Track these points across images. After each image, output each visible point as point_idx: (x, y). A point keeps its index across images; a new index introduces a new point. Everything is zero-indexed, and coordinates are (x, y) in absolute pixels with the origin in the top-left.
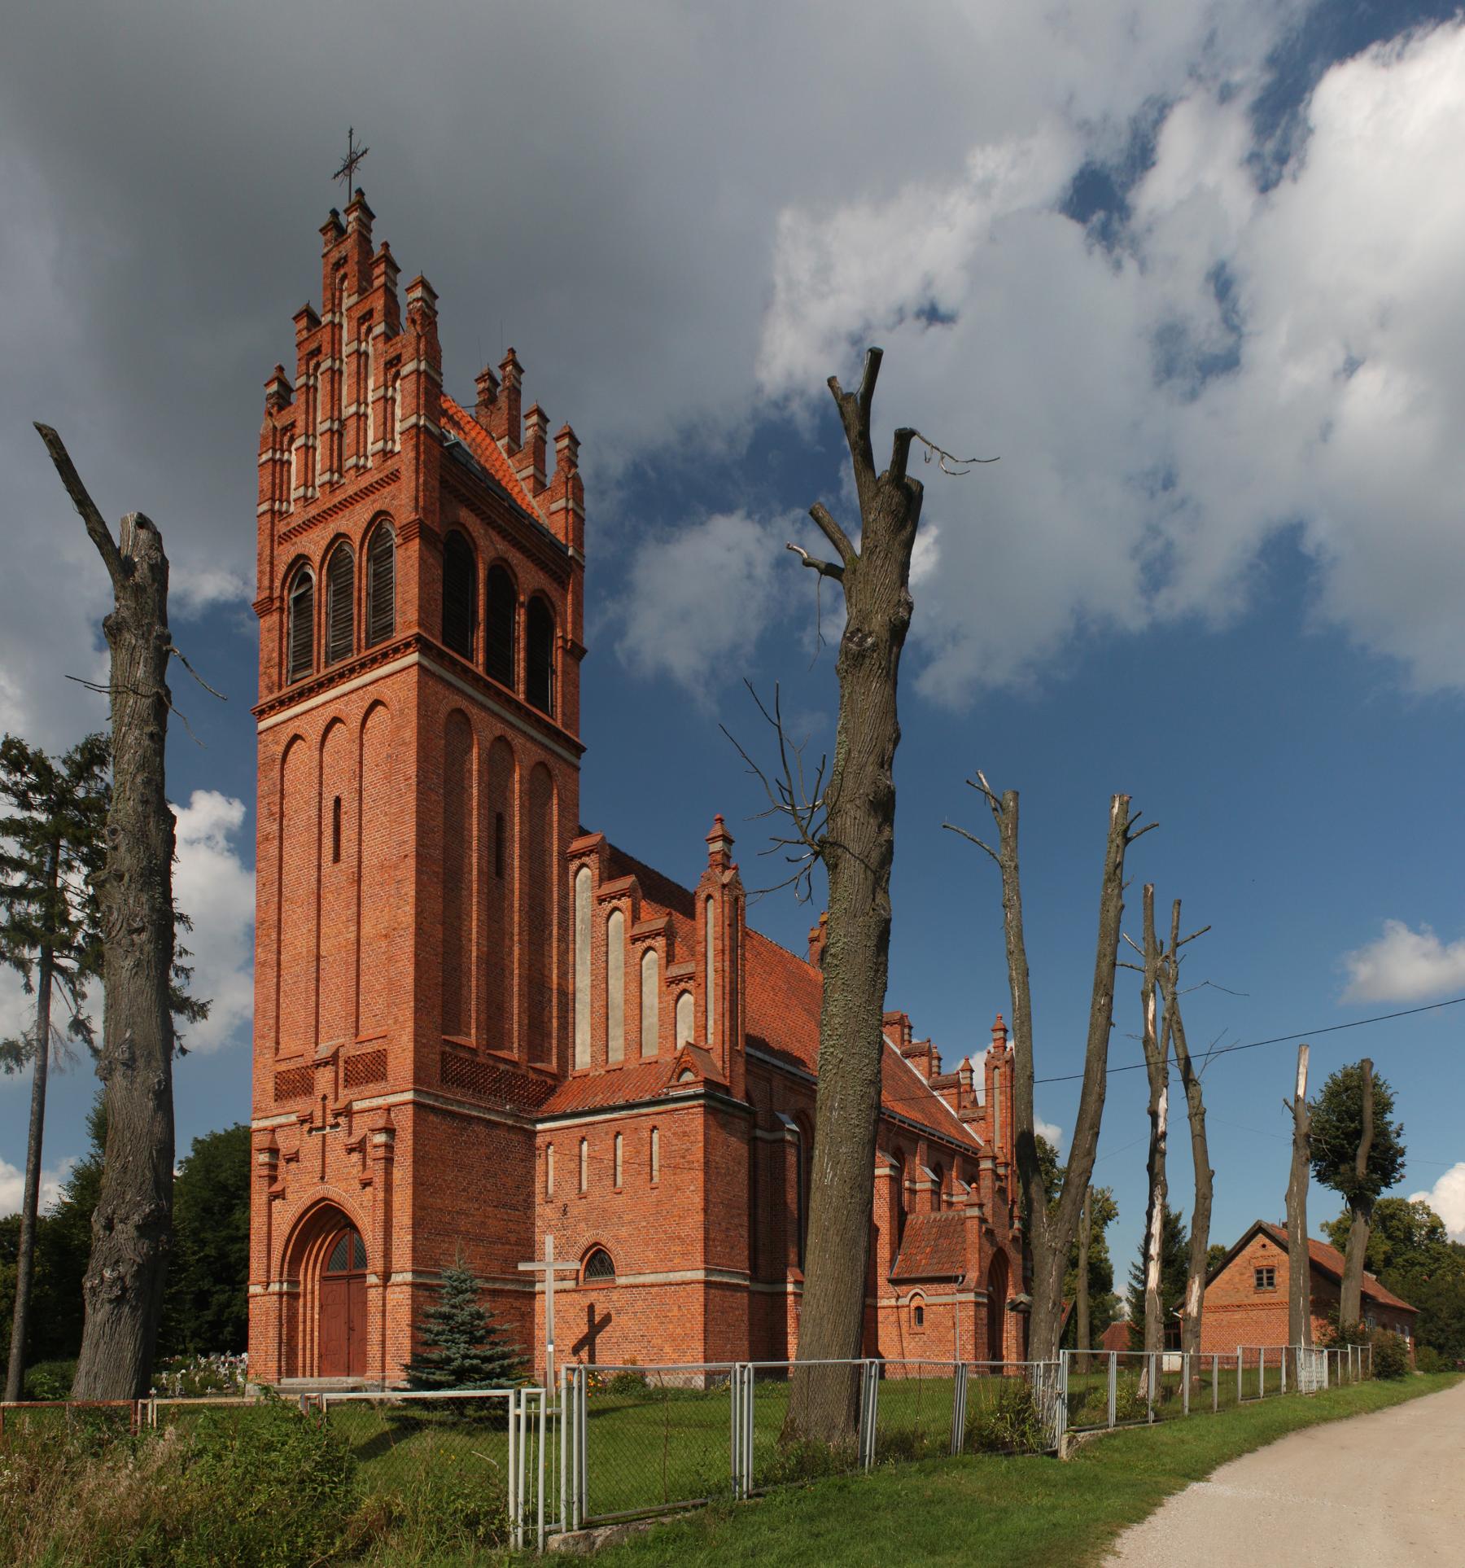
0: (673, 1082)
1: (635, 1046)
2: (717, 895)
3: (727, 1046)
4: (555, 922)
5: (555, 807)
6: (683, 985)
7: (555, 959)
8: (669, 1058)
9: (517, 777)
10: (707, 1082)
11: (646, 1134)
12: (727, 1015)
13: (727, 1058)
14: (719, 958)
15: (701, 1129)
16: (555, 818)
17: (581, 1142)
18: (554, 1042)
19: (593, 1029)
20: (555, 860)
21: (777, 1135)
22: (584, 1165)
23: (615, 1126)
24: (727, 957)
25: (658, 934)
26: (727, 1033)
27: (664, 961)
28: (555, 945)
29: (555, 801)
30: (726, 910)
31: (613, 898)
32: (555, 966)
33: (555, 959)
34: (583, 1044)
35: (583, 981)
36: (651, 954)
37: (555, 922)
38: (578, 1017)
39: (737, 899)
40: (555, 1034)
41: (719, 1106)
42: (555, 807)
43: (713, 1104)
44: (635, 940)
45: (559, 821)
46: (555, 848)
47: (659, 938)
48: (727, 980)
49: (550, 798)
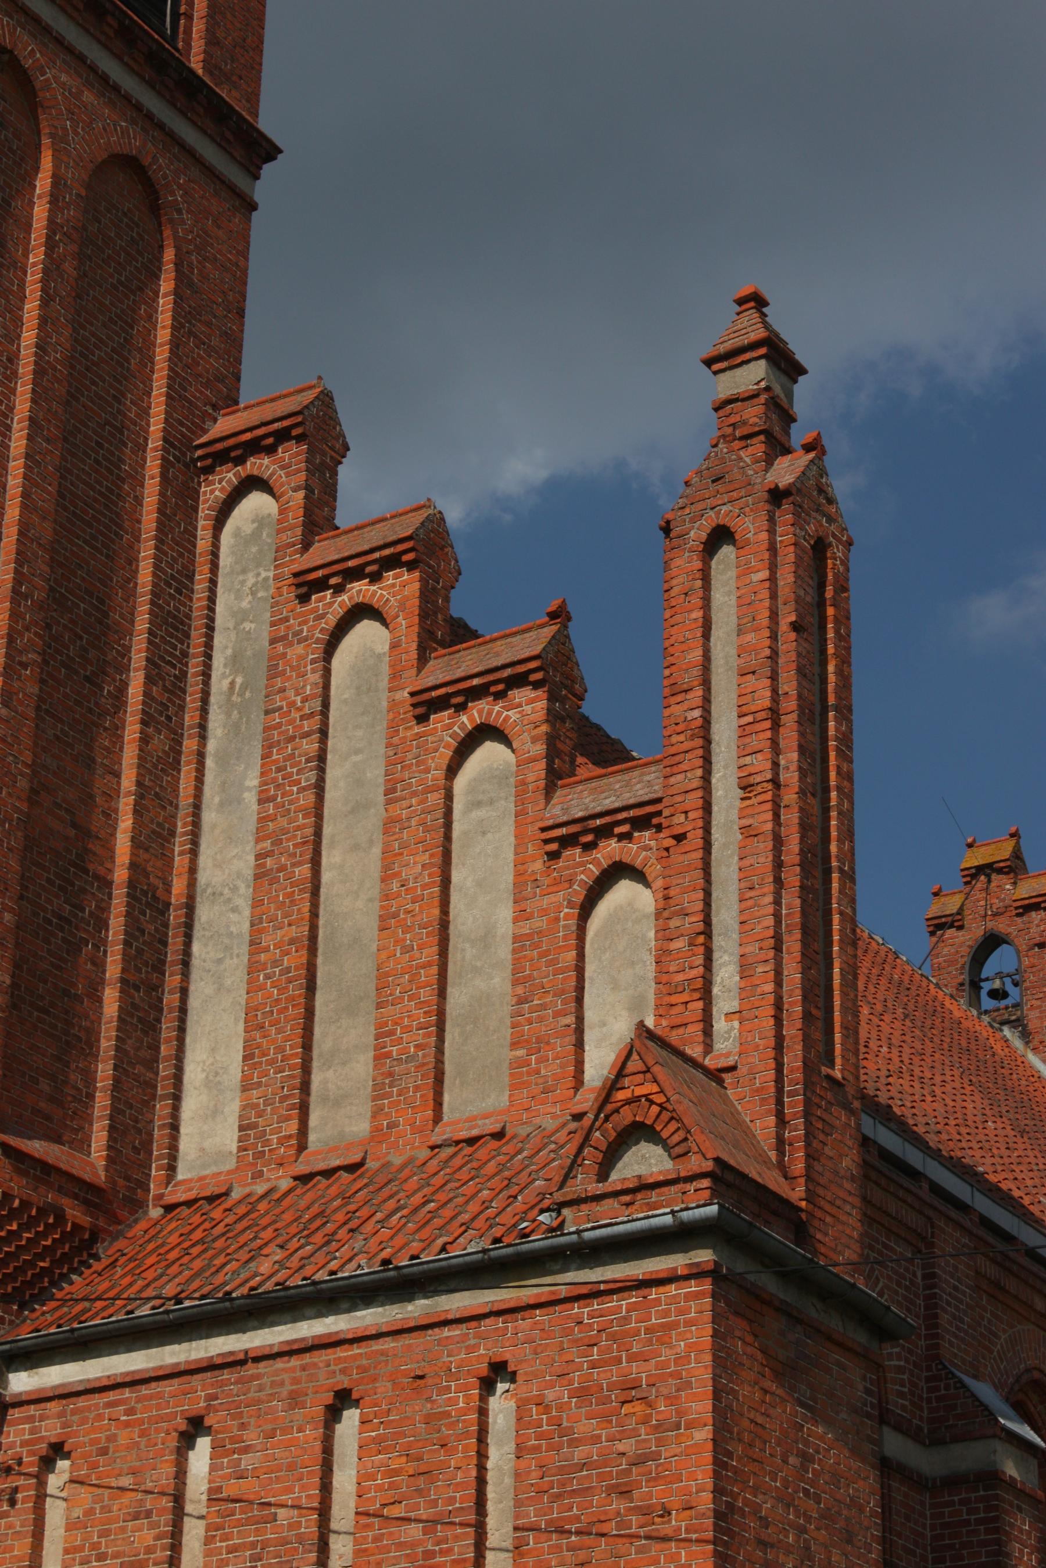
0: (584, 1183)
1: (414, 1081)
2: (751, 527)
3: (794, 1059)
4: (138, 657)
5: (165, 305)
6: (610, 850)
7: (128, 781)
8: (550, 1117)
9: (43, 183)
10: (725, 1178)
11: (461, 1399)
12: (793, 943)
13: (794, 1106)
14: (761, 739)
15: (701, 1371)
16: (163, 335)
17: (187, 1440)
18: (104, 1071)
19: (253, 1024)
20: (153, 465)
21: (965, 1457)
22: (194, 1532)
23: (327, 1372)
24: (789, 735)
25: (518, 681)
26: (794, 1007)
27: (537, 772)
28: (132, 731)
29: (166, 285)
30: (786, 578)
31: (354, 574)
32: (126, 805)
33: (128, 781)
34: (212, 1084)
35: (225, 864)
36: (490, 752)
37: (138, 657)
38: (200, 989)
39: (820, 547)
40: (107, 1043)
41: (769, 1283)
42: (165, 305)
43: (740, 1265)
44: (427, 705)
45: (175, 345)
46: (156, 425)
47: (521, 695)
48: (791, 818)
49: (154, 275)
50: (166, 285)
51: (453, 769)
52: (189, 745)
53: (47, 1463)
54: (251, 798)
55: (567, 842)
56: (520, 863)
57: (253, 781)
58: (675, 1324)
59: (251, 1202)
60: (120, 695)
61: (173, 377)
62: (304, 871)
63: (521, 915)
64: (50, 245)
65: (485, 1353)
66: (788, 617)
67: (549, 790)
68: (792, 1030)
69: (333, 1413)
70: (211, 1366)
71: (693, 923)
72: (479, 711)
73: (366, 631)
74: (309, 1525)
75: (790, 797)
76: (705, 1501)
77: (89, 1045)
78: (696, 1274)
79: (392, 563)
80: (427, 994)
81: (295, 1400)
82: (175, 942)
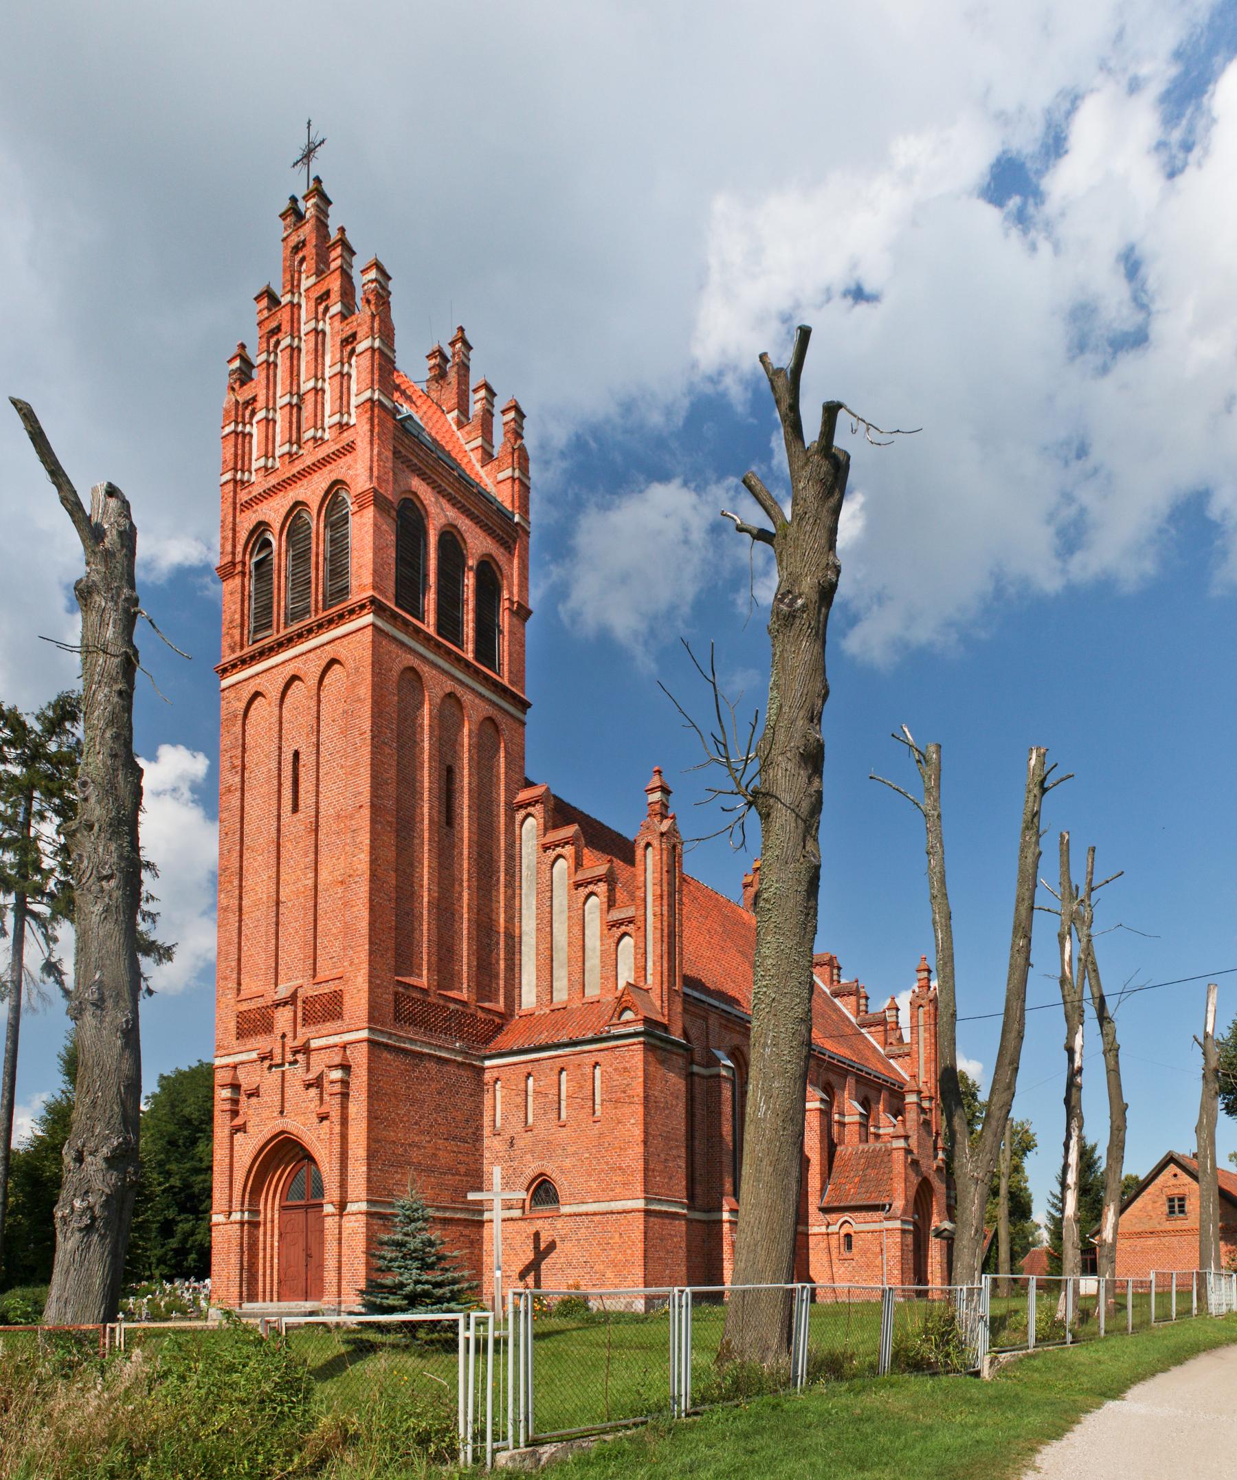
0: (615, 1021)
1: (578, 986)
2: (656, 843)
3: (665, 986)
4: (502, 869)
5: (502, 760)
6: (623, 928)
8: (610, 998)
9: (466, 731)
10: (647, 1020)
11: (588, 1070)
12: (665, 957)
14: (658, 903)
15: (641, 1065)
16: (502, 770)
17: (527, 1078)
18: (502, 983)
21: (713, 1071)
22: (530, 1099)
23: (559, 1063)
24: (665, 901)
25: (600, 880)
27: (605, 906)
28: (502, 890)
29: (502, 754)
30: (665, 857)
31: (558, 846)
32: (502, 910)
33: (502, 904)
35: (529, 925)
40: (502, 975)
41: (658, 1043)
42: (502, 760)
45: (506, 773)
46: (502, 798)
47: (601, 884)
48: (665, 924)
50: (502, 754)
51: (584, 903)
52: (517, 892)
53: (495, 1082)
54: (534, 907)
55: (613, 926)
56: (602, 930)
57: (534, 903)
58: (635, 1055)
59: (540, 1016)
60: (498, 880)
61: (506, 783)
62: (548, 929)
63: (602, 945)
64: (470, 751)
65: (594, 1059)
66: (665, 869)
67: (608, 911)
68: (665, 979)
69: (560, 1073)
70: (532, 1061)
71: (642, 951)
72: (591, 888)
73: (561, 861)
74: (556, 1098)
75: (665, 918)
76: (642, 1095)
77: (497, 976)
78: (640, 1043)
79: (567, 843)
80: (580, 964)
81: (551, 1069)
82: (517, 946)
